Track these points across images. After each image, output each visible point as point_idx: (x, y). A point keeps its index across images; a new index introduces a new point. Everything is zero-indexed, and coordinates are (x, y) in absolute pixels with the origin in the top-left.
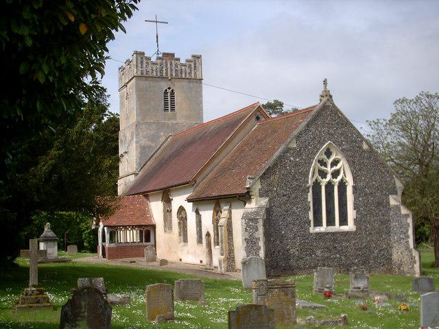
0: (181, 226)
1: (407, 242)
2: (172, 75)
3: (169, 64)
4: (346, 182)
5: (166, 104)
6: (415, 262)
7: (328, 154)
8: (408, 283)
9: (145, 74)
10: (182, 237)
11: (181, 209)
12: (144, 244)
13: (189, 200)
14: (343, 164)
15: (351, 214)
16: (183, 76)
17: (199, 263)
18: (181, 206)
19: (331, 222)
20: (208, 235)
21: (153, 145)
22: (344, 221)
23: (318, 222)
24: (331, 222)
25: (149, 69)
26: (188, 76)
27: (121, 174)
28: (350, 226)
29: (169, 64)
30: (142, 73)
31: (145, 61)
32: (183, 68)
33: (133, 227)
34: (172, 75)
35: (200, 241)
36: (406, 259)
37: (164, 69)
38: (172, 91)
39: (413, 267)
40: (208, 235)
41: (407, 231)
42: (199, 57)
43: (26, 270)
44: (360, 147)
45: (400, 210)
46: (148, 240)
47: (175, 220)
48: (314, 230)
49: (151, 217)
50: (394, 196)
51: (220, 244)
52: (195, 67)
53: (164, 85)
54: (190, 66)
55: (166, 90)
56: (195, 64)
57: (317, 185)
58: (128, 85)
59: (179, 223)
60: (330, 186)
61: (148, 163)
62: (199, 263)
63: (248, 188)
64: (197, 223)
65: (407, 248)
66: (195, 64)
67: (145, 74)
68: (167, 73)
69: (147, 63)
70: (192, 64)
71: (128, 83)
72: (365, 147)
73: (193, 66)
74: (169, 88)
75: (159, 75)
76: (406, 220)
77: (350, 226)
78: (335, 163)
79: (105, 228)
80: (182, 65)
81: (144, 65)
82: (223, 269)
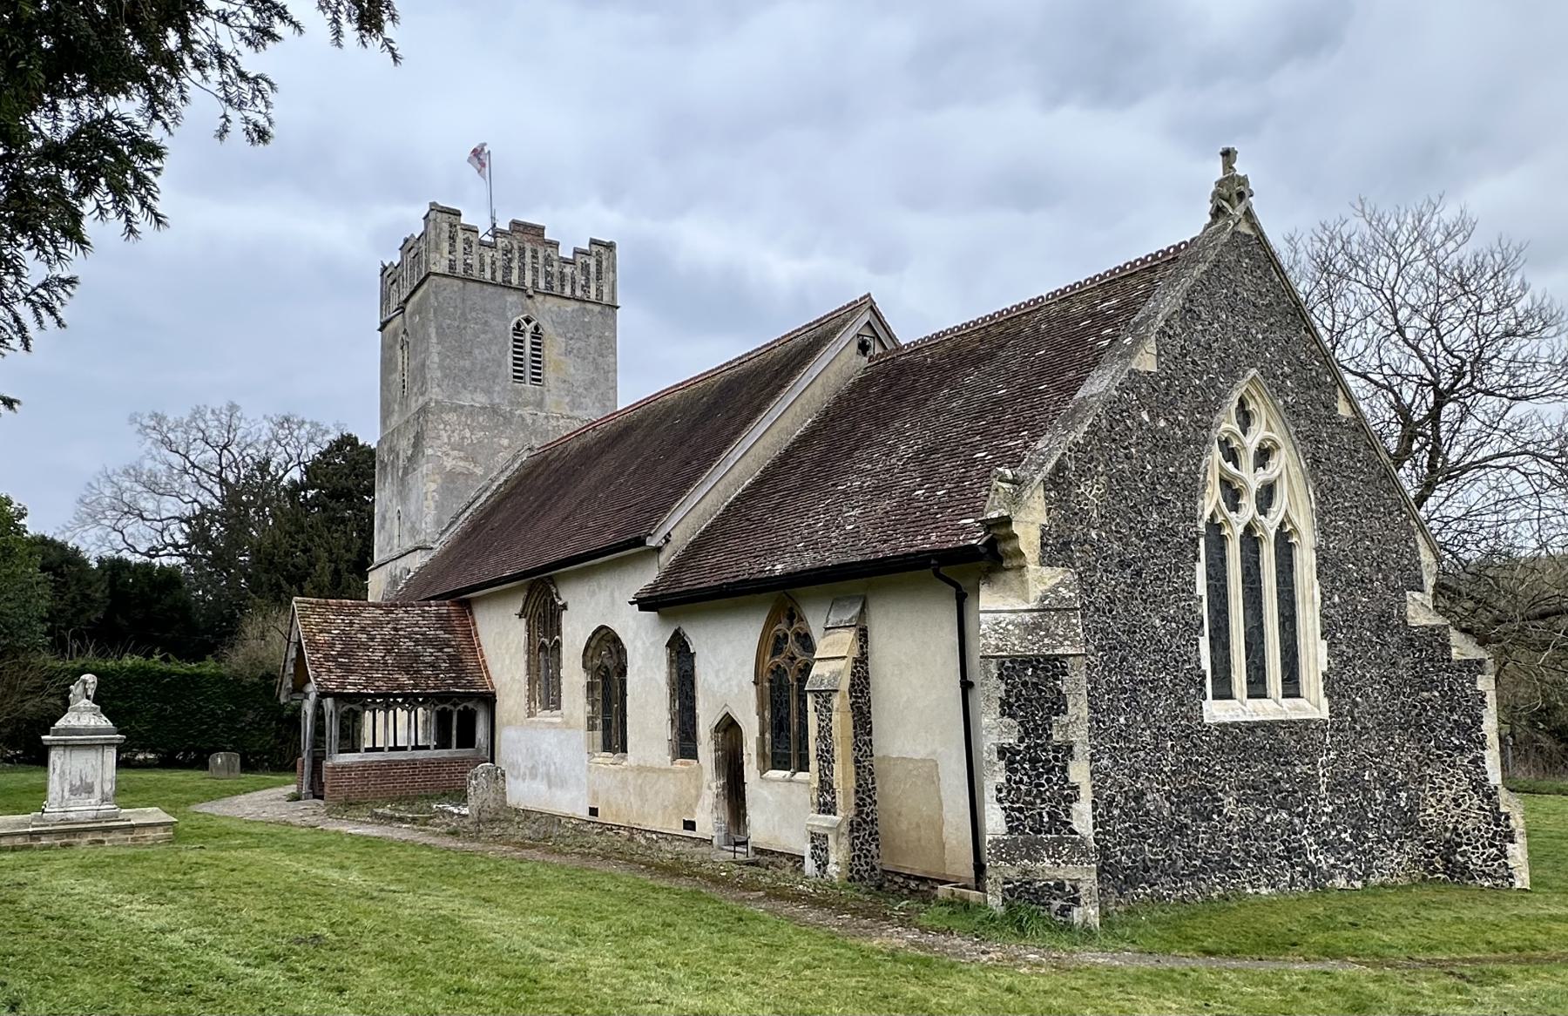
0: (598, 695)
1: (1478, 762)
2: (535, 283)
3: (528, 254)
4: (1295, 530)
5: (518, 362)
6: (1072, 798)
7: (1245, 418)
8: (1382, 885)
9: (460, 269)
10: (598, 734)
11: (606, 645)
12: (453, 752)
13: (645, 603)
14: (1284, 463)
15: (1315, 656)
16: (568, 291)
17: (677, 828)
18: (602, 628)
19: (1257, 688)
20: (729, 728)
21: (479, 471)
22: (1291, 686)
23: (1224, 691)
24: (1257, 688)
25: (474, 260)
26: (579, 293)
27: (377, 559)
28: (1313, 705)
29: (528, 254)
30: (452, 267)
31: (461, 236)
32: (568, 270)
33: (411, 701)
34: (535, 283)
35: (685, 745)
36: (1473, 819)
37: (515, 264)
38: (537, 328)
39: (1503, 853)
40: (729, 728)
41: (1478, 721)
42: (610, 247)
43: (1047, 560)
44: (1330, 407)
45: (1446, 647)
46: (467, 740)
47: (574, 677)
48: (1215, 711)
49: (482, 668)
50: (1417, 595)
51: (814, 765)
52: (599, 272)
53: (513, 309)
54: (585, 267)
55: (519, 325)
56: (599, 264)
57: (1214, 527)
58: (409, 308)
59: (591, 687)
60: (1251, 540)
61: (462, 518)
62: (677, 828)
63: (989, 525)
64: (672, 684)
65: (1479, 785)
66: (599, 264)
67: (460, 269)
68: (522, 276)
69: (467, 242)
70: (592, 262)
71: (406, 301)
72: (1343, 410)
73: (593, 269)
74: (528, 321)
75: (499, 279)
76: (1474, 683)
77: (1313, 705)
78: (1263, 455)
79: (329, 703)
80: (566, 262)
81: (460, 245)
82: (832, 869)
